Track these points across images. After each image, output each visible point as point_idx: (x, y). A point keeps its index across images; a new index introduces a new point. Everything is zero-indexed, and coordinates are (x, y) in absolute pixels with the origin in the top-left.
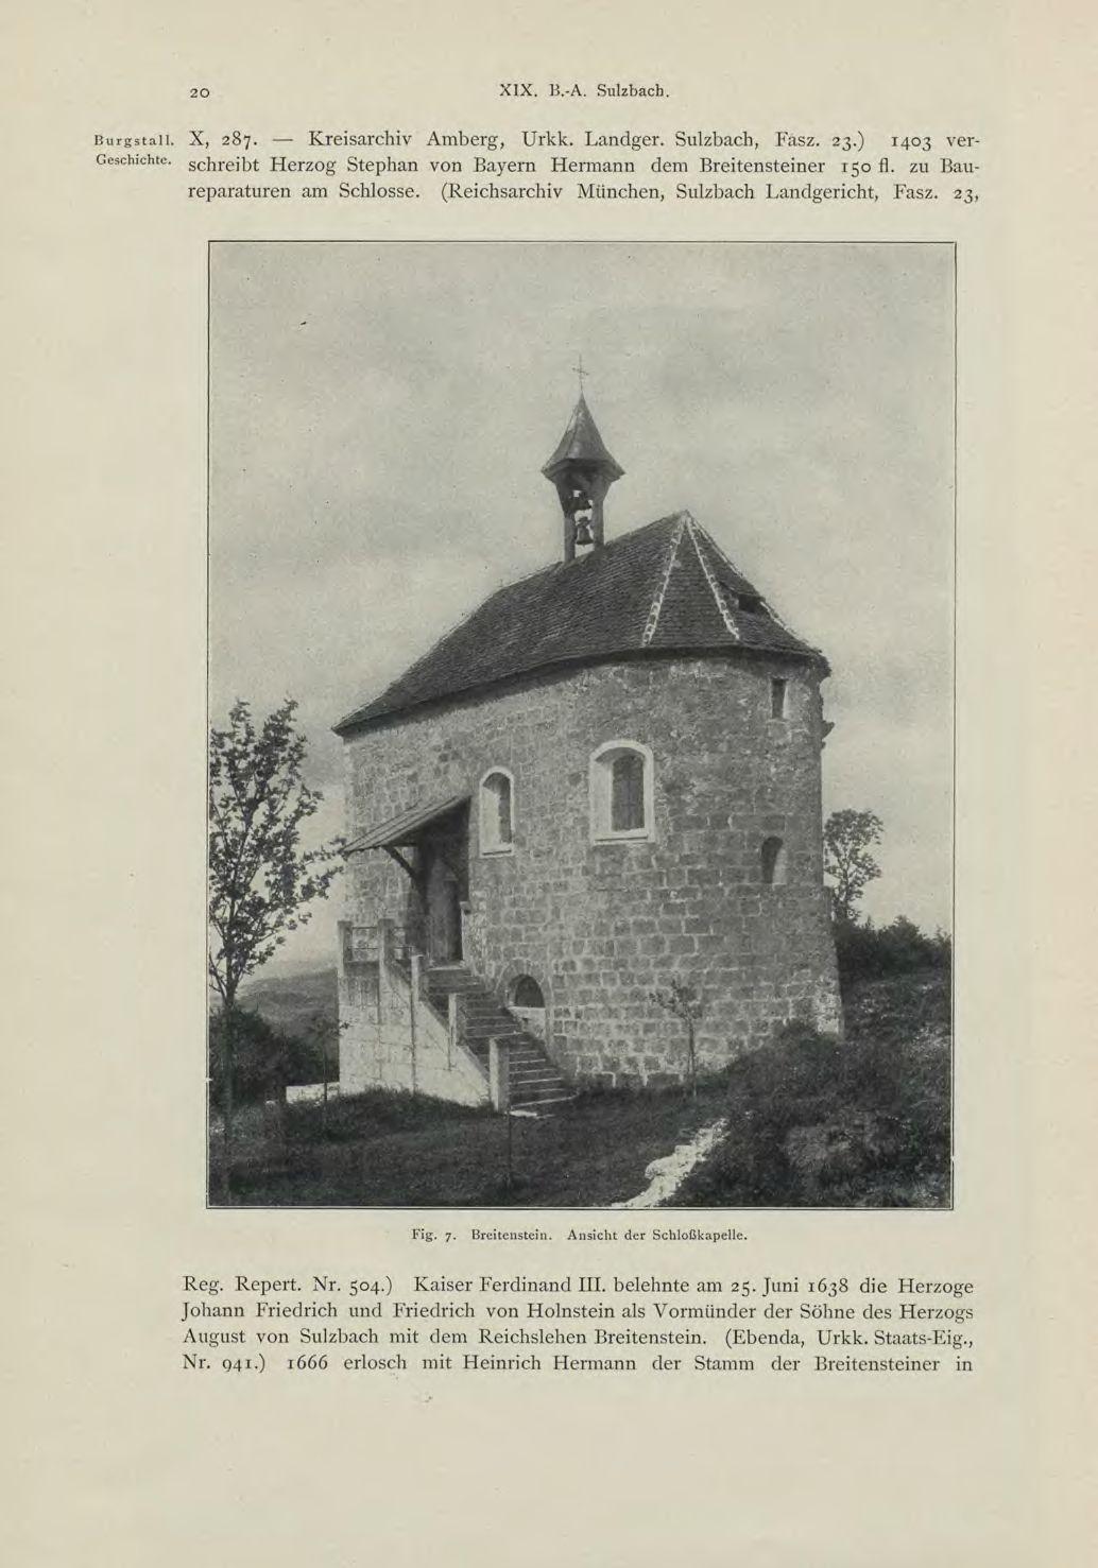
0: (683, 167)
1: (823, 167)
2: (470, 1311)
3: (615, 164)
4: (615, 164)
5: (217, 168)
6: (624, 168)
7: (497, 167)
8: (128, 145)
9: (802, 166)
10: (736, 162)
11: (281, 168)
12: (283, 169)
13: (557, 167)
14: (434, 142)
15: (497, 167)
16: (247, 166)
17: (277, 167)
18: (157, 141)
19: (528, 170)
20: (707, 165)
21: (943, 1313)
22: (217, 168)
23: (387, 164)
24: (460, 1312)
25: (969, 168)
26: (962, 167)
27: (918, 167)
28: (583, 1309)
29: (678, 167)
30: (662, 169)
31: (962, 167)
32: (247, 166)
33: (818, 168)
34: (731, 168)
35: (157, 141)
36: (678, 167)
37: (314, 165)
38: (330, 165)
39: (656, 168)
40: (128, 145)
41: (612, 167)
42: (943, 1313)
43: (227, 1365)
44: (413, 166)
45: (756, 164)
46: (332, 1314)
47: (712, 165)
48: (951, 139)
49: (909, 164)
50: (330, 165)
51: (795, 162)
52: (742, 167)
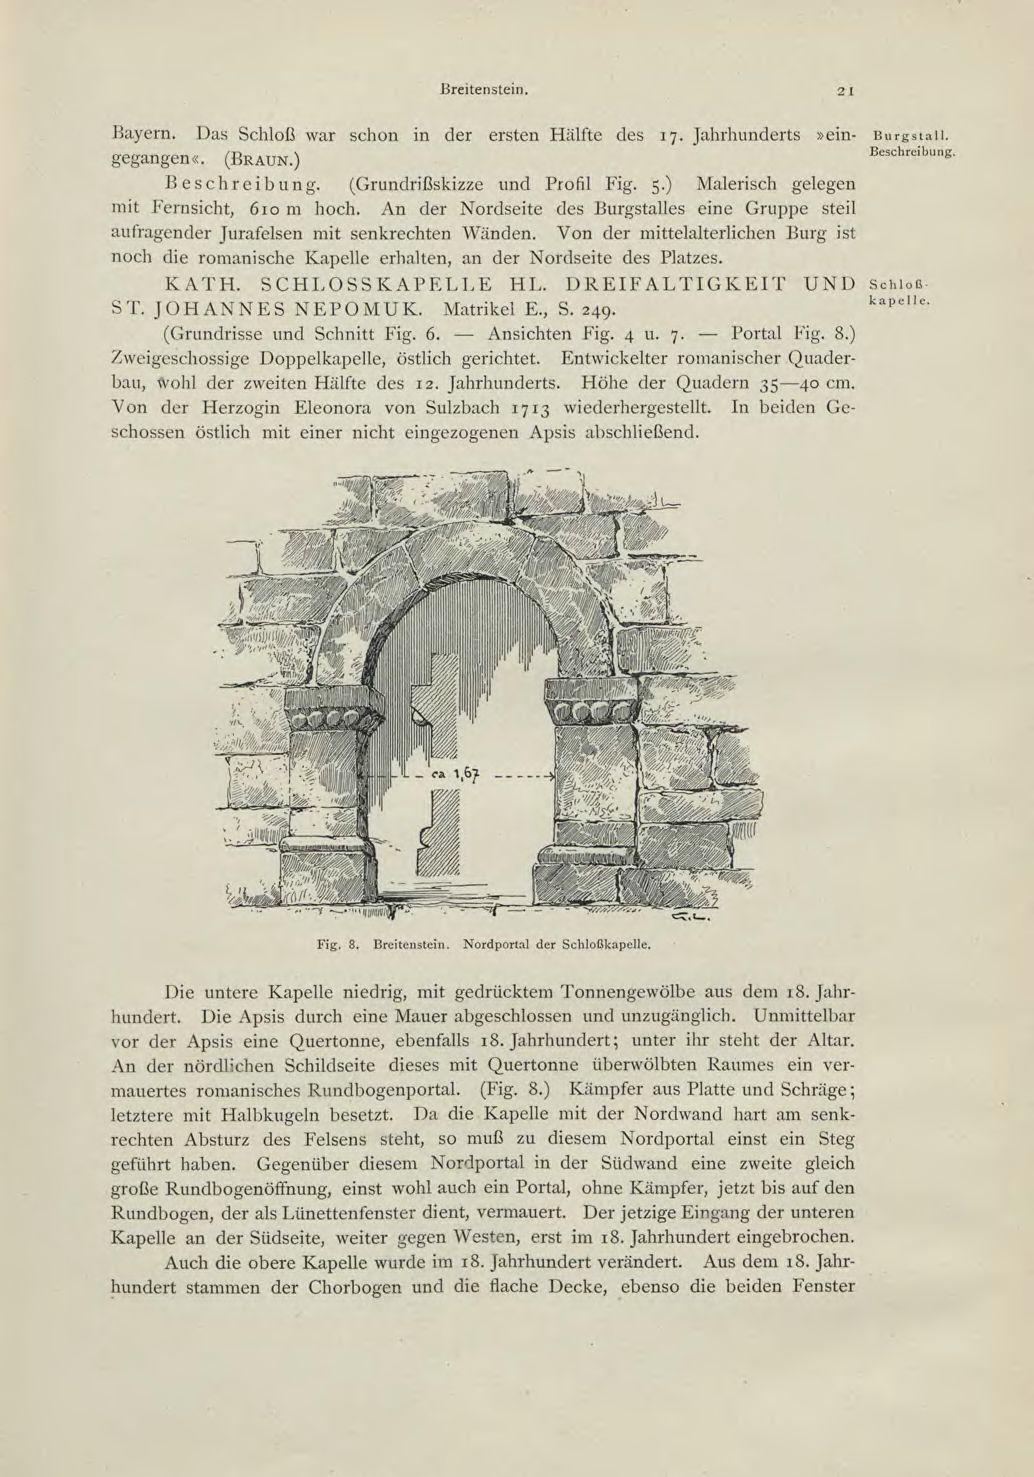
0: (549, 994)
1: (613, 1213)
2: (447, 359)
3: (244, 257)
4: (244, 257)
5: (476, 386)
6: (225, 1289)
7: (134, 134)
8: (905, 140)
9: (373, 1017)
10: (280, 379)
11: (591, 386)
12: (214, 412)
13: (229, 281)
14: (495, 337)
15: (134, 134)
16: (665, 1065)
17: (556, 137)
18: (933, 137)
19: (163, 137)
20: (321, 1193)
21: (700, 259)
22: (476, 386)
23: (592, 1187)
24: (437, 360)
25: (850, 1189)
26: (662, 1090)
27: (525, 1139)
28: (832, 206)
29: (543, 993)
30: (216, 386)
31: (662, 1090)
32: (665, 1065)
33: (777, 1214)
34: (591, 260)
35: (933, 137)
36: (543, 993)
37: (474, 185)
38: (745, 1212)
39: (608, 235)
40: (905, 140)
41: (209, 1289)
42: (700, 259)
43: (267, 434)
44: (200, 1239)
45: (619, 991)
46: (446, 362)
47: (243, 159)
48: (390, 407)
49: (516, 1135)
50: (745, 1212)
51: (356, 1185)
52: (370, 1239)
